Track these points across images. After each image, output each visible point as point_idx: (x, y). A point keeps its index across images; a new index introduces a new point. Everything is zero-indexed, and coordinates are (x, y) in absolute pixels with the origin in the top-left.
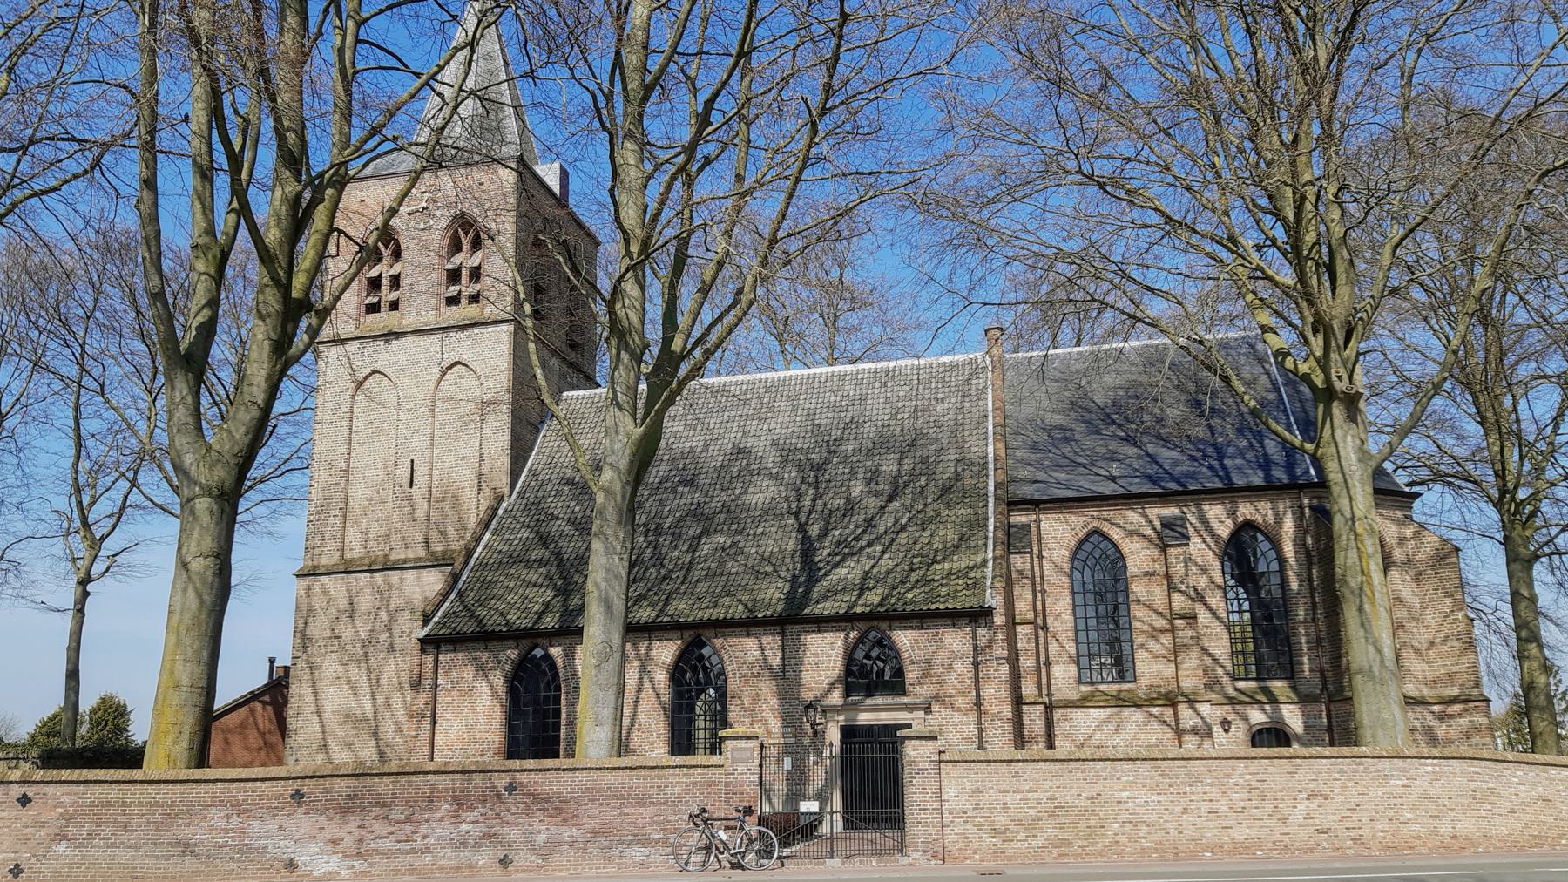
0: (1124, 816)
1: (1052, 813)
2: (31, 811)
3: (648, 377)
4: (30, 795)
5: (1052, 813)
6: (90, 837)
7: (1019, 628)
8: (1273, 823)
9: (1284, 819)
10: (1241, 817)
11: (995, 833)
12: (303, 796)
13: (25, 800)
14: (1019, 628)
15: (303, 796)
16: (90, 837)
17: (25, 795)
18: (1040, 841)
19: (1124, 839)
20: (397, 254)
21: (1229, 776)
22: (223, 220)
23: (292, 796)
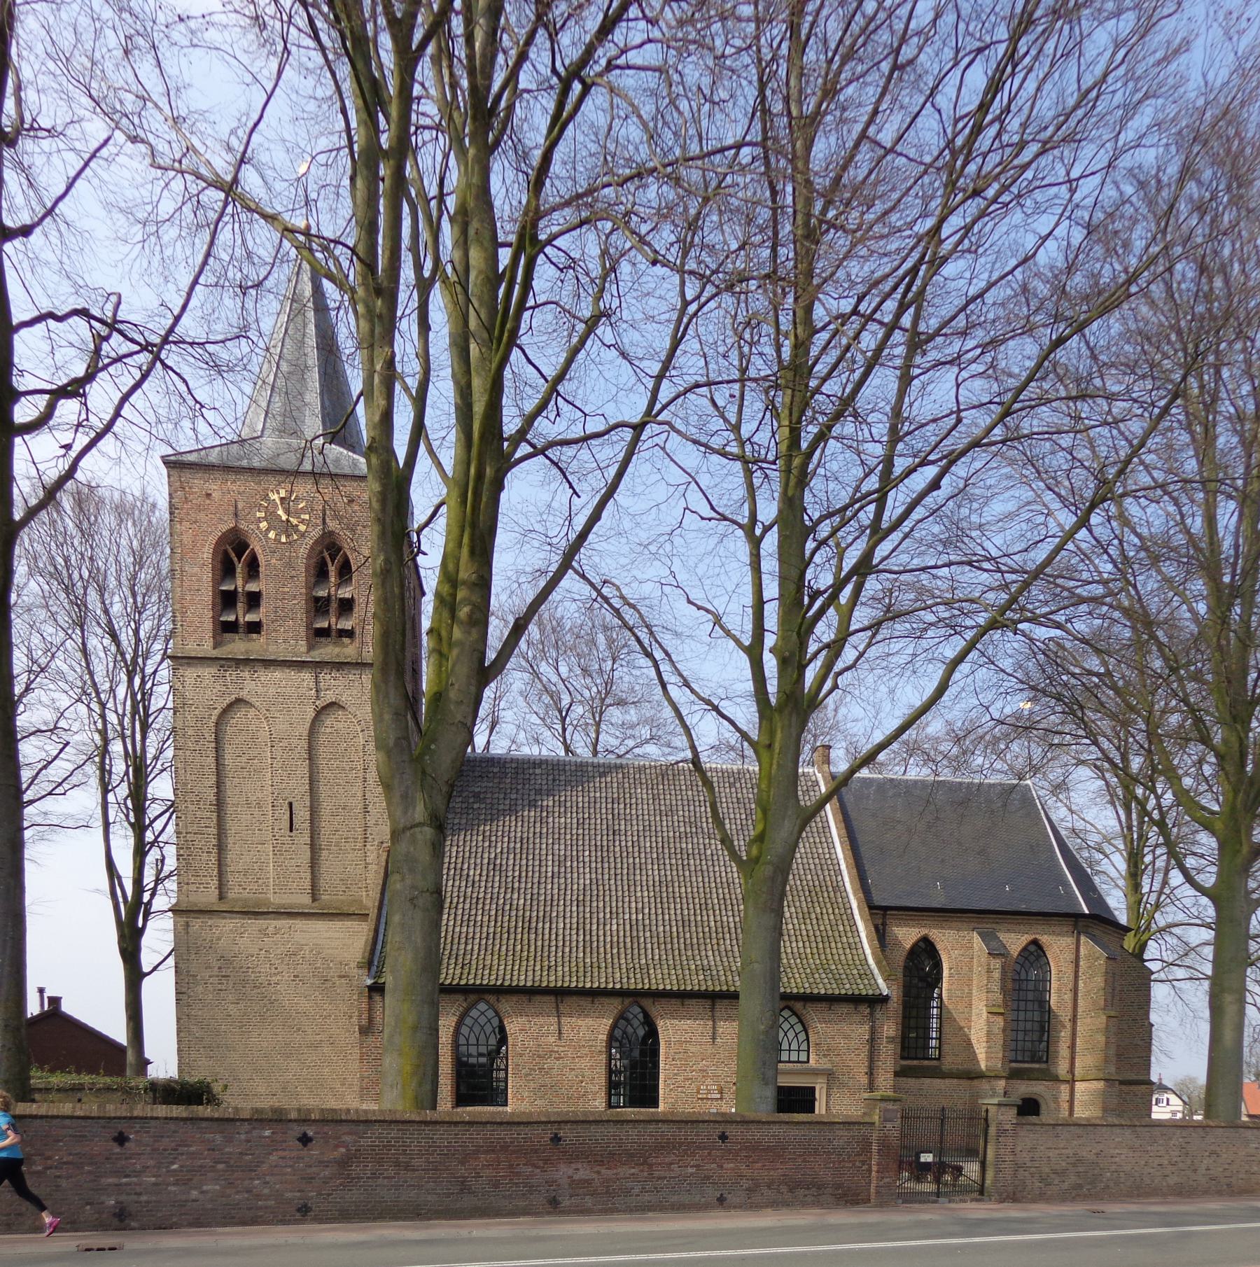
0: (1114, 1167)
1: (1074, 1165)
2: (314, 1151)
3: (933, 999)
4: (311, 1134)
5: (1074, 1165)
6: (374, 1176)
7: (500, 250)
8: (1189, 1173)
9: (1195, 1171)
10: (1174, 1168)
11: (1042, 1180)
12: (560, 1139)
13: (305, 1140)
14: (500, 250)
15: (560, 1139)
16: (374, 1176)
17: (305, 1134)
18: (1066, 1186)
19: (1112, 1184)
20: (253, 568)
21: (1170, 1139)
22: (860, 640)
23: (552, 1139)
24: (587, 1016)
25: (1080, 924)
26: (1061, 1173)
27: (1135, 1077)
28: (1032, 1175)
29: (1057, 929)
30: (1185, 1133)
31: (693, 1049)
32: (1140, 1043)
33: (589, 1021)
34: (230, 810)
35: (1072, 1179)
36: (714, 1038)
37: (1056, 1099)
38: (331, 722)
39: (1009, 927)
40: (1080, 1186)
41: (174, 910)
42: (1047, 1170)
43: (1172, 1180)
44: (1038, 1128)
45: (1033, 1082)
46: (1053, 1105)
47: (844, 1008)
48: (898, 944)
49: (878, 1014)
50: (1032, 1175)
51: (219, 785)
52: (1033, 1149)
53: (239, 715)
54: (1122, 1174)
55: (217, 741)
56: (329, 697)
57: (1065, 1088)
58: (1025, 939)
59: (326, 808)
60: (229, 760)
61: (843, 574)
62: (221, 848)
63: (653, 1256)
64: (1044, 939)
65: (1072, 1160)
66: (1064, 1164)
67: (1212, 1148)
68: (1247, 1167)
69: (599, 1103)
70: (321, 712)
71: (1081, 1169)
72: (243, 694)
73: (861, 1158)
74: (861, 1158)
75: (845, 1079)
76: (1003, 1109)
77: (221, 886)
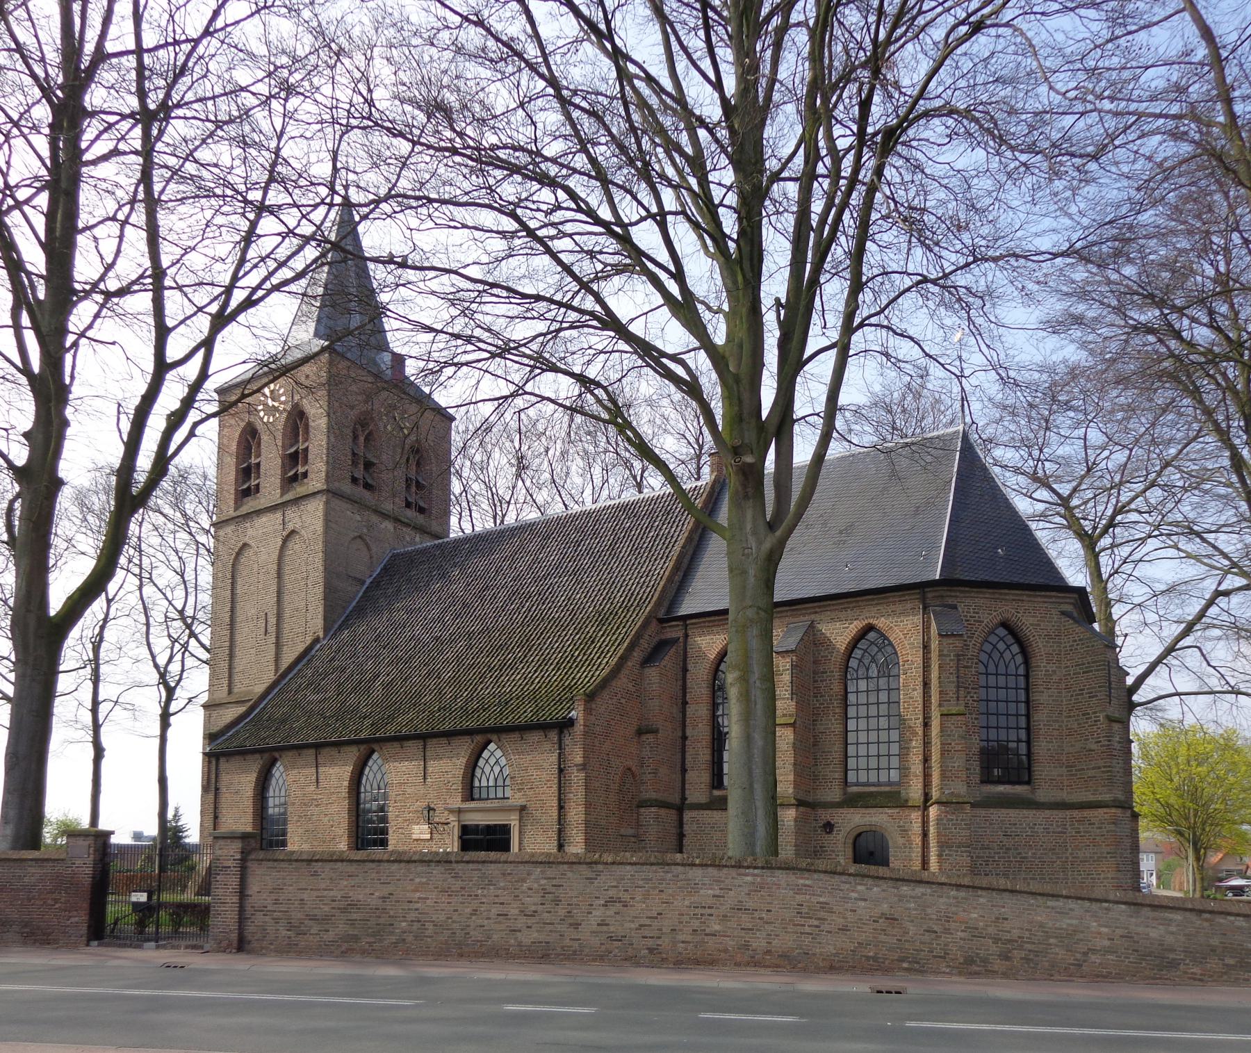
1: (344, 910)
9: (576, 925)
19: (410, 938)
24: (336, 765)
25: (930, 595)
26: (327, 919)
27: (1091, 798)
28: (277, 921)
29: (899, 608)
30: (550, 872)
31: (409, 791)
32: (1094, 747)
33: (337, 769)
34: (238, 625)
35: (341, 928)
36: (425, 778)
37: (904, 831)
38: (295, 545)
39: (833, 615)
40: (356, 938)
41: (205, 706)
42: (299, 915)
43: (528, 937)
44: (283, 865)
45: (872, 811)
46: (901, 841)
47: (535, 737)
48: (702, 655)
49: (567, 740)
50: (277, 921)
51: (233, 610)
52: (277, 890)
53: (248, 553)
54: (430, 926)
55: (233, 577)
56: (290, 527)
57: (916, 816)
58: (854, 627)
59: (287, 613)
60: (239, 590)
61: (229, 310)
62: (231, 656)
63: (1006, 1028)
64: (881, 623)
65: (343, 904)
66: (326, 909)
67: (612, 893)
68: (696, 924)
69: (343, 846)
70: (285, 540)
71: (354, 916)
72: (246, 540)
73: (54, 896)
74: (54, 896)
75: (538, 814)
76: (221, 842)
77: (230, 686)
